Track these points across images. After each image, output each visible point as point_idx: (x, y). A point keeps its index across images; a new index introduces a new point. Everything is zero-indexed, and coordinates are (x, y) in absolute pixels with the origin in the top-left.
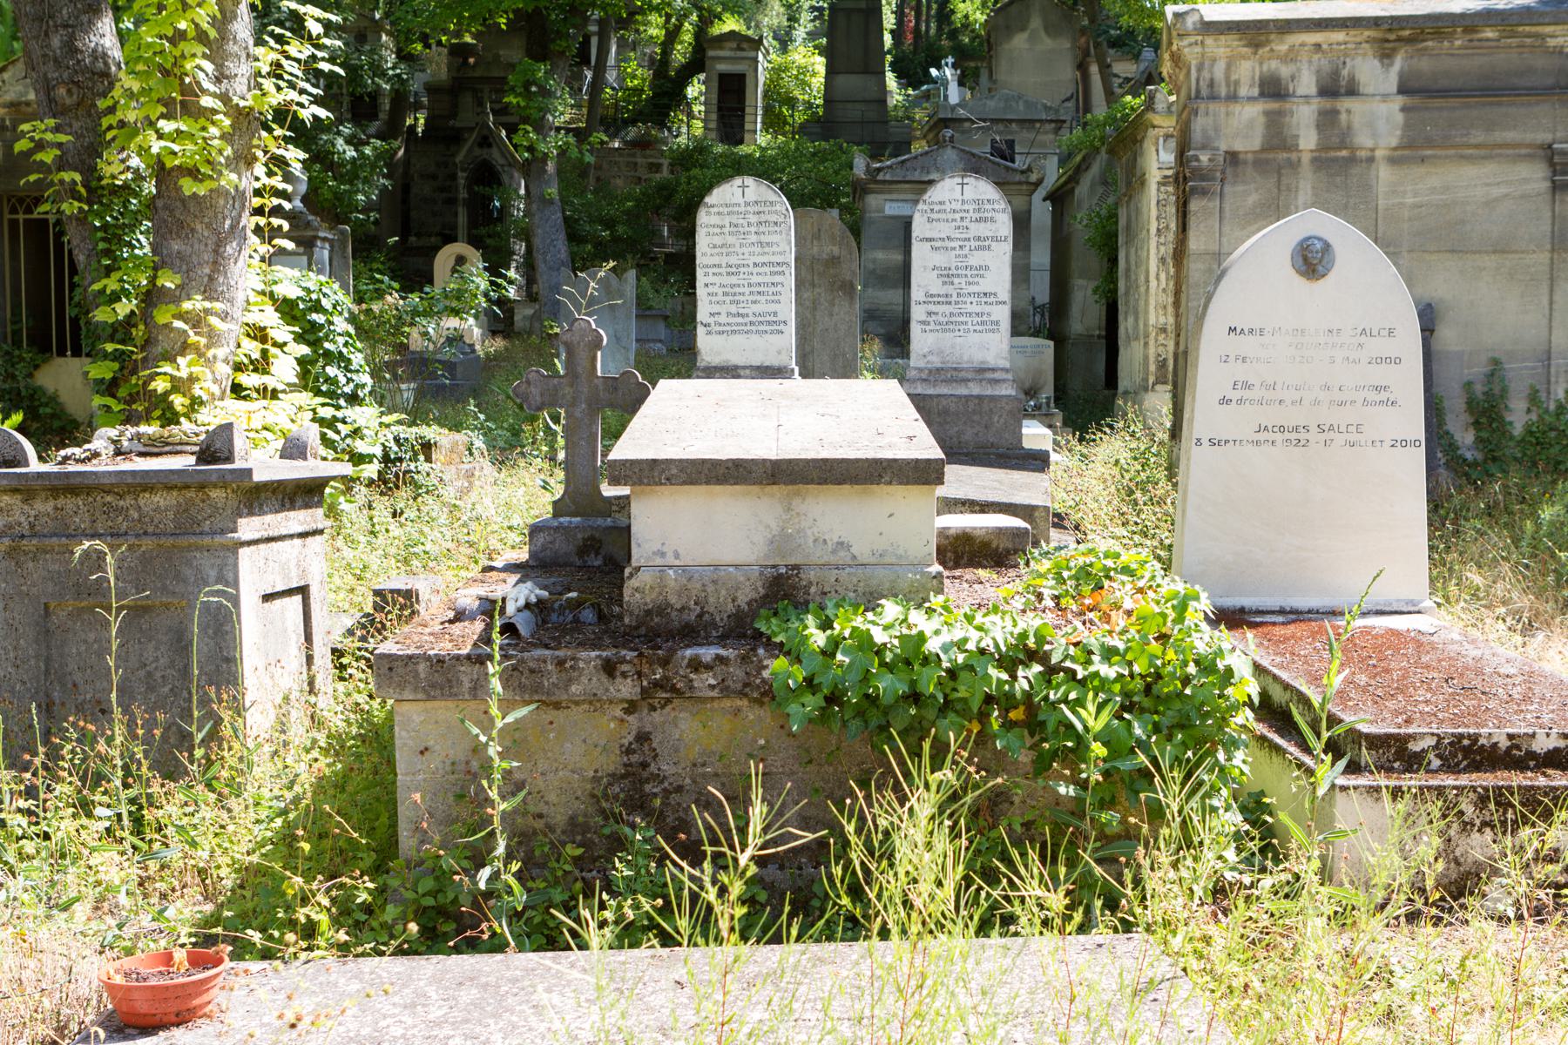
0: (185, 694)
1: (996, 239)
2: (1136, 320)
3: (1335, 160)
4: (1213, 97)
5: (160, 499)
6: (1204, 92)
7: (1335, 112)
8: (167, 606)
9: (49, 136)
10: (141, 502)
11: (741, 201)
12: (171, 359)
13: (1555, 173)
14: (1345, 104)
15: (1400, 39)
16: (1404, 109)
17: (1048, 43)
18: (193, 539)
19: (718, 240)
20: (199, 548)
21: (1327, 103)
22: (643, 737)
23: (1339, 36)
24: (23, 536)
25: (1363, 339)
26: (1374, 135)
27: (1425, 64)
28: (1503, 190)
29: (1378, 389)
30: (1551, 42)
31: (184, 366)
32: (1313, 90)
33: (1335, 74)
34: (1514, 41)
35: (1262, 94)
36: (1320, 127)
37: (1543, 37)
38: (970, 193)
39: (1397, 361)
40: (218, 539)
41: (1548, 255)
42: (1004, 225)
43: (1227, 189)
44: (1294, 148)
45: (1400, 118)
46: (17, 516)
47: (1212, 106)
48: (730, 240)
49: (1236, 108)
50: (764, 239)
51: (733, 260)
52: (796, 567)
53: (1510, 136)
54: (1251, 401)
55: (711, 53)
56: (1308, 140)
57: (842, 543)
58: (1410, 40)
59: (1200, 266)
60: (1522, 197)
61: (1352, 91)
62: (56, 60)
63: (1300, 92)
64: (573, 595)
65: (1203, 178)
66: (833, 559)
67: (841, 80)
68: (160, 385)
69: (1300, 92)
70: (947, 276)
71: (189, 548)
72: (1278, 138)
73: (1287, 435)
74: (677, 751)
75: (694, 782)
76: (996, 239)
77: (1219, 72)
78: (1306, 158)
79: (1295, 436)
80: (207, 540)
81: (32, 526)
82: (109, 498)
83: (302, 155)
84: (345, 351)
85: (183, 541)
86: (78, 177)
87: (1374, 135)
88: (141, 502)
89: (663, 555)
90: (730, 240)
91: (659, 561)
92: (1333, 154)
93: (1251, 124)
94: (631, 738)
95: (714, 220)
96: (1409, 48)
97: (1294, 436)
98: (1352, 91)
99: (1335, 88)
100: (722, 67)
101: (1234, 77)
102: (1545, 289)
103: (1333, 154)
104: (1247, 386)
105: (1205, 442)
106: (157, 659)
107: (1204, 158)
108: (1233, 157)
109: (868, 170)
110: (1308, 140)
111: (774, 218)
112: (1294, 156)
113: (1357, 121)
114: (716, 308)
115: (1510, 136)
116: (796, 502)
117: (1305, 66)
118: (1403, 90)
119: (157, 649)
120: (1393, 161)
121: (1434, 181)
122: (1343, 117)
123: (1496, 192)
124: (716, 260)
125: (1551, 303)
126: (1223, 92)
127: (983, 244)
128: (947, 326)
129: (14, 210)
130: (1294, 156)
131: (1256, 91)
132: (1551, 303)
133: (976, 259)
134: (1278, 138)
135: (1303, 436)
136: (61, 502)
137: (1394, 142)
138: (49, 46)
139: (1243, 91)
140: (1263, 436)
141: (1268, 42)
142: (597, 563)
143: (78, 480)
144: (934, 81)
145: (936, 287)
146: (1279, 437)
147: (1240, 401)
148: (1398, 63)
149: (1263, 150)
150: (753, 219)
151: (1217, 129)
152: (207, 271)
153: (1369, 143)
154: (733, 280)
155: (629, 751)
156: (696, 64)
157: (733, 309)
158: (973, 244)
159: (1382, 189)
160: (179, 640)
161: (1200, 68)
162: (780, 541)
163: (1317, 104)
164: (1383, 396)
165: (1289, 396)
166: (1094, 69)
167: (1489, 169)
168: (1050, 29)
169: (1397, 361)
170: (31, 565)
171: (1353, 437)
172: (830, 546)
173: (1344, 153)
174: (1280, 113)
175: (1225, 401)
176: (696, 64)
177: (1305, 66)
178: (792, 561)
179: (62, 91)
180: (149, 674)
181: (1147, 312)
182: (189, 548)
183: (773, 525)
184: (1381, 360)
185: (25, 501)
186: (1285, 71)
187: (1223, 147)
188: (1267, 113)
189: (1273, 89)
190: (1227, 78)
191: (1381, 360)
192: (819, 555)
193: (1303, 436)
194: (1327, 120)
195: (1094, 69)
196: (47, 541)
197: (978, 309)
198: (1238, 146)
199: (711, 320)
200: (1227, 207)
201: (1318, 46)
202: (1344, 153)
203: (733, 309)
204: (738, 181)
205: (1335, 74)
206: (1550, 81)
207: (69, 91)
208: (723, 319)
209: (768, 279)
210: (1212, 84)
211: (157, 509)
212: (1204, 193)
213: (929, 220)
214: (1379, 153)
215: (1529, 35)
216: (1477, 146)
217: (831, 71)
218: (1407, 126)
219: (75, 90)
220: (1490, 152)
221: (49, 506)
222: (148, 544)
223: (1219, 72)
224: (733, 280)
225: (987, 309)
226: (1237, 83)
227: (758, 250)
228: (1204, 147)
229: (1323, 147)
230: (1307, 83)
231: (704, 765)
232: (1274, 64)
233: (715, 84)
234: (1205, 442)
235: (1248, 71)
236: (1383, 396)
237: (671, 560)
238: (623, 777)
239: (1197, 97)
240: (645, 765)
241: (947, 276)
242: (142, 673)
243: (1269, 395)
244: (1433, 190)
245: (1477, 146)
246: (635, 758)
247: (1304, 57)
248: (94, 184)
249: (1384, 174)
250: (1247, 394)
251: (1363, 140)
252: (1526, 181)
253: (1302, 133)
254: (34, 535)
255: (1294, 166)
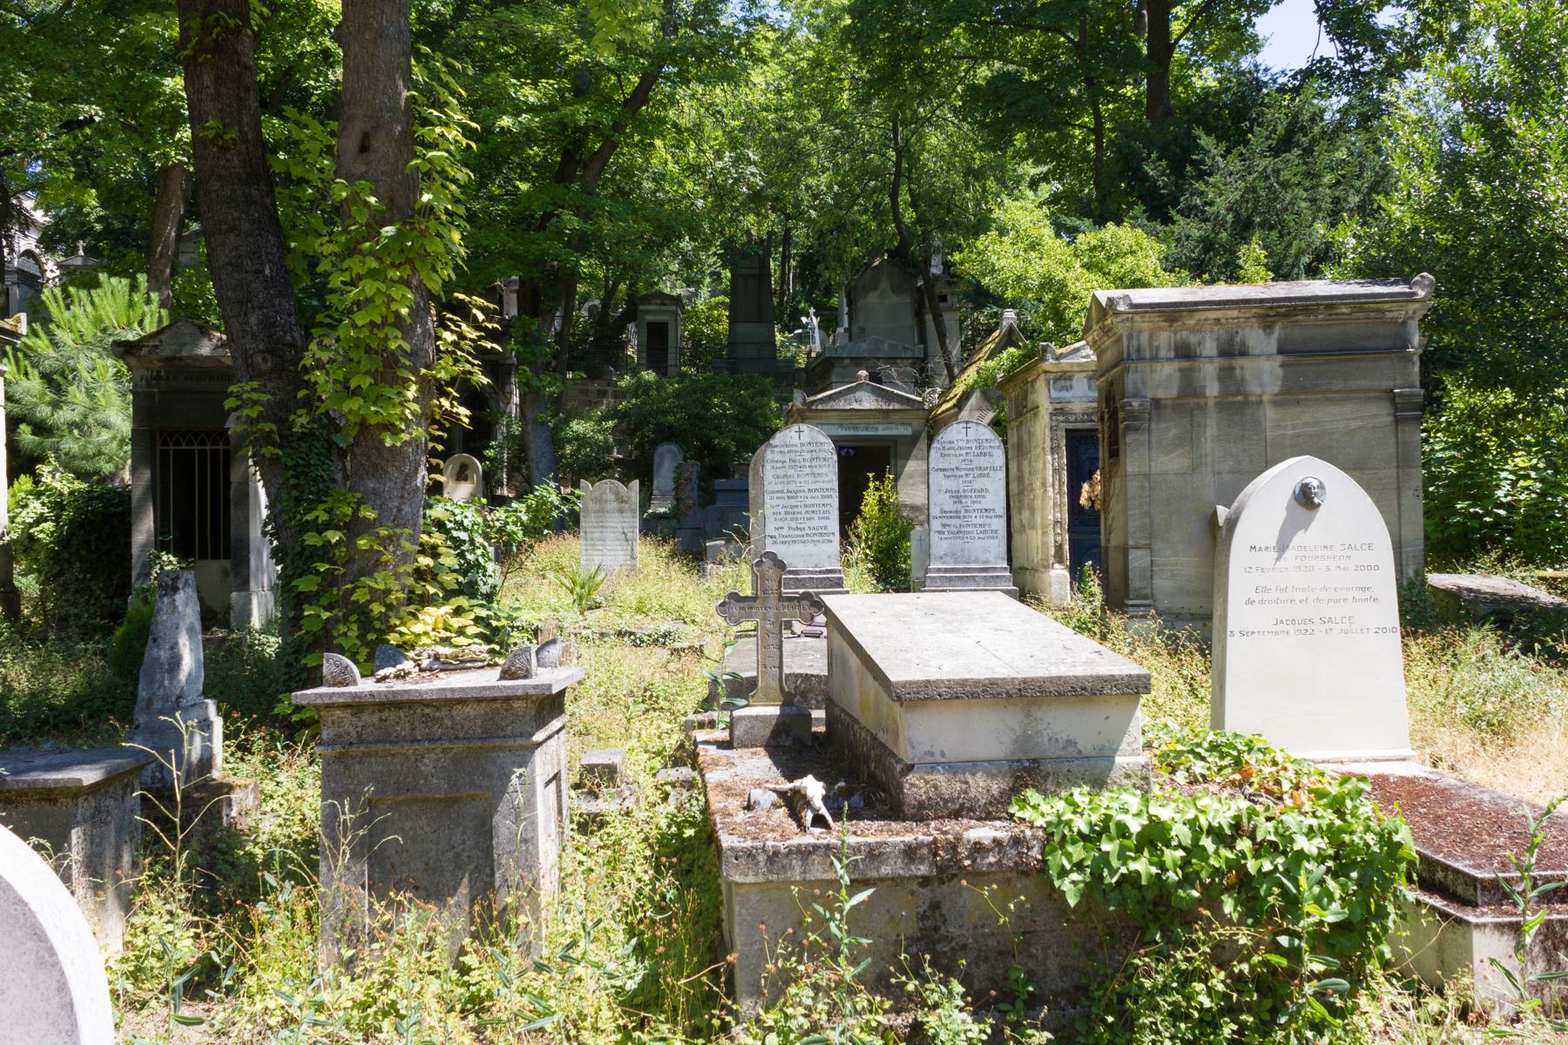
0: (488, 870)
1: (993, 469)
2: (1033, 514)
3: (1233, 403)
4: (1141, 359)
5: (469, 710)
6: (1134, 355)
7: (1231, 369)
8: (473, 798)
9: (255, 396)
10: (454, 713)
11: (797, 442)
12: (370, 574)
13: (1396, 410)
14: (1239, 362)
15: (1278, 315)
16: (1282, 365)
17: (893, 299)
18: (498, 742)
19: (780, 472)
20: (501, 749)
21: (1225, 362)
22: (935, 906)
23: (1235, 313)
24: (351, 744)
25: (1349, 552)
26: (1261, 385)
27: (1296, 332)
28: (1359, 423)
29: (1363, 589)
30: (1390, 315)
31: (379, 582)
32: (1215, 352)
33: (1231, 341)
34: (1362, 315)
35: (1177, 356)
36: (1221, 379)
37: (1382, 311)
38: (972, 434)
39: (1376, 567)
40: (520, 741)
41: (1394, 471)
42: (999, 458)
43: (1153, 426)
44: (1202, 395)
45: (1280, 372)
46: (347, 727)
47: (1140, 365)
48: (790, 472)
49: (1158, 366)
50: (816, 471)
51: (792, 487)
52: (1035, 761)
53: (1363, 383)
54: (1270, 602)
55: (642, 307)
56: (1212, 389)
57: (1069, 741)
58: (1285, 315)
59: (1135, 484)
60: (1373, 428)
61: (1244, 353)
62: (253, 335)
63: (1205, 353)
64: (842, 784)
65: (1135, 418)
66: (1063, 753)
67: (743, 328)
68: (360, 596)
69: (1205, 353)
70: (957, 497)
71: (494, 749)
72: (1190, 387)
73: (1298, 627)
74: (961, 916)
75: (975, 940)
76: (993, 469)
77: (1144, 339)
78: (1211, 403)
79: (1304, 627)
80: (510, 742)
81: (359, 735)
82: (427, 711)
83: (468, 413)
84: (481, 560)
85: (490, 744)
86: (275, 428)
87: (1261, 385)
88: (454, 713)
89: (932, 754)
90: (790, 472)
91: (929, 759)
92: (1231, 399)
93: (1169, 377)
94: (925, 907)
95: (778, 457)
96: (1285, 321)
97: (1302, 627)
98: (1244, 353)
99: (1231, 351)
100: (650, 318)
101: (1155, 344)
102: (1395, 496)
103: (1231, 399)
104: (1265, 589)
105: (1237, 633)
106: (464, 842)
107: (1136, 404)
108: (1157, 403)
109: (804, 403)
110: (1212, 389)
111: (822, 455)
112: (1202, 401)
113: (1248, 376)
114: (780, 524)
115: (1363, 383)
116: (1034, 709)
117: (1208, 336)
118: (1280, 352)
119: (464, 833)
120: (1275, 403)
121: (1307, 418)
122: (1238, 371)
123: (1354, 425)
124: (779, 487)
125: (1399, 506)
126: (1148, 354)
127: (983, 472)
128: (959, 533)
129: (165, 443)
130: (1202, 401)
131: (1172, 354)
132: (1399, 506)
133: (978, 484)
134: (1190, 387)
135: (1309, 627)
136: (385, 714)
137: (1276, 390)
138: (246, 323)
139: (1163, 354)
140: (1280, 628)
141: (1181, 317)
142: (788, 743)
143: (405, 697)
144: (804, 327)
145: (949, 505)
146: (1291, 628)
147: (1262, 601)
148: (1277, 333)
149: (1179, 397)
150: (807, 456)
151: (1144, 383)
152: (396, 503)
153: (1258, 390)
154: (793, 502)
155: (923, 918)
156: (631, 315)
157: (793, 524)
158: (976, 472)
159: (1269, 425)
160: (484, 825)
161: (1130, 337)
162: (1022, 741)
163: (1218, 362)
164: (1367, 595)
165: (1299, 596)
166: (929, 318)
167: (1347, 408)
168: (896, 289)
169: (1376, 567)
170: (357, 767)
171: (1346, 626)
172: (1061, 743)
173: (1240, 398)
174: (1191, 370)
175: (1250, 602)
176: (631, 315)
177: (1208, 336)
178: (1032, 756)
179: (259, 359)
180: (457, 855)
181: (1043, 509)
182: (494, 749)
183: (1017, 728)
184: (1363, 568)
185: (354, 715)
186: (1193, 339)
187: (1149, 395)
188: (1181, 370)
189: (1185, 352)
190: (1150, 344)
191: (1363, 568)
192: (1052, 751)
193: (1309, 627)
194: (1226, 374)
195: (929, 318)
196: (374, 748)
197: (980, 521)
198: (1161, 394)
199: (776, 533)
200: (1154, 439)
201: (1218, 320)
202: (1240, 398)
203: (793, 524)
204: (795, 428)
205: (1231, 341)
206: (1389, 343)
207: (264, 359)
208: (785, 532)
209: (820, 501)
210: (1139, 349)
211: (467, 718)
212: (1136, 429)
213: (942, 455)
214: (1265, 398)
215: (1373, 310)
216: (1338, 392)
217: (733, 319)
218: (1285, 378)
219: (269, 357)
220: (1347, 396)
221: (375, 718)
222: (459, 746)
223: (1144, 339)
224: (793, 502)
225: (987, 521)
226: (1158, 348)
227: (811, 479)
228: (1135, 396)
229: (1224, 394)
230: (1210, 347)
231: (983, 926)
232: (1185, 334)
233: (644, 331)
234: (1237, 633)
235: (1165, 339)
236: (1367, 595)
237: (938, 758)
238: (919, 939)
239: (1129, 358)
240: (936, 929)
241: (957, 497)
242: (451, 854)
243: (1283, 596)
244: (1307, 424)
245: (1338, 392)
246: (929, 923)
247: (1207, 328)
248: (286, 433)
249: (1270, 413)
250: (1266, 596)
251: (1254, 389)
252: (1375, 416)
253: (1208, 384)
254: (360, 742)
255: (1203, 408)
